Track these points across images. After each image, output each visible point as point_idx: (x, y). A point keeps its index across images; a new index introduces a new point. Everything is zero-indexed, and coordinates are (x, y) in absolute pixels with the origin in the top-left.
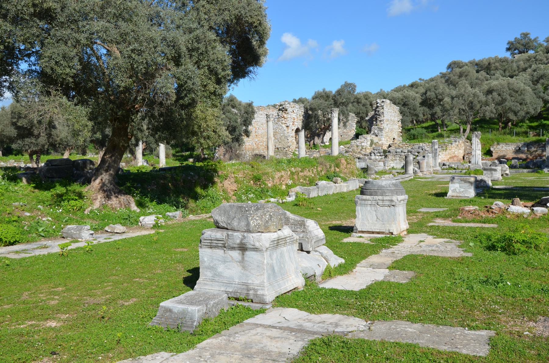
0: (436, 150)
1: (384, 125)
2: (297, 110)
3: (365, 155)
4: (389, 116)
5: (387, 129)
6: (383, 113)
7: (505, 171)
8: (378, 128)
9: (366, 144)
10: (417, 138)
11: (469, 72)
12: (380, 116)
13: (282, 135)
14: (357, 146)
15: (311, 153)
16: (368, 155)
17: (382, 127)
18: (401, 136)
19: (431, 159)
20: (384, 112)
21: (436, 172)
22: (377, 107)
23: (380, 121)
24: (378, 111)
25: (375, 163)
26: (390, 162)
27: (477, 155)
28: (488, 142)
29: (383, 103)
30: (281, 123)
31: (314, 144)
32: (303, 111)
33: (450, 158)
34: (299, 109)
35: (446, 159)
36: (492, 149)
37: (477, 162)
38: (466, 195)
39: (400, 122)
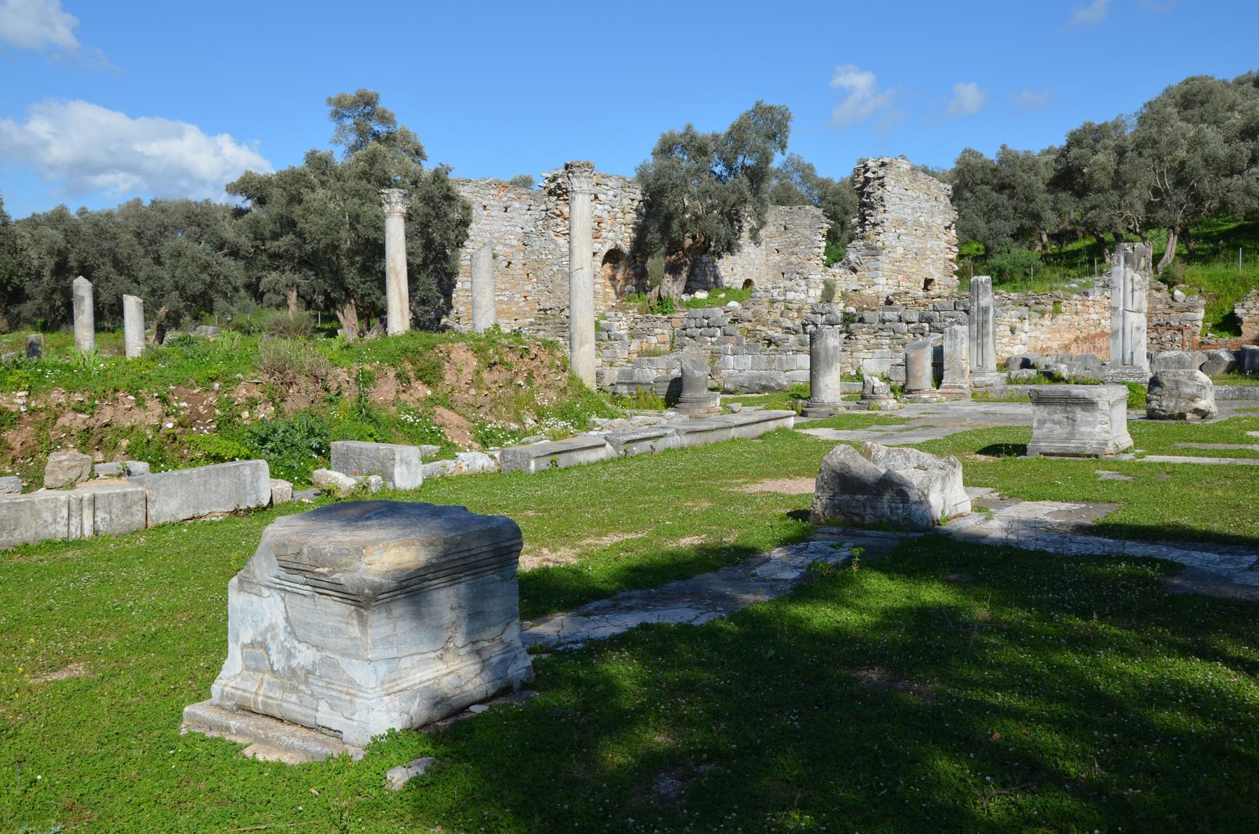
0: (985, 311)
1: (887, 238)
2: (611, 193)
3: (788, 330)
4: (910, 211)
5: (900, 250)
6: (882, 199)
7: (1193, 398)
8: (868, 247)
9: (803, 296)
10: (1012, 279)
11: (1210, 93)
12: (872, 208)
13: (555, 268)
14: (773, 302)
15: (648, 325)
16: (797, 332)
17: (880, 244)
18: (956, 273)
19: (966, 344)
20: (886, 197)
21: (981, 394)
22: (867, 180)
23: (875, 225)
24: (869, 194)
25: (784, 357)
26: (862, 355)
27: (1128, 330)
28: (1229, 290)
29: (883, 169)
30: (552, 234)
31: (660, 298)
32: (640, 197)
33: (1076, 340)
34: (619, 191)
35: (1055, 345)
36: (1239, 311)
37: (1128, 357)
38: (325, 716)
39: (953, 232)
